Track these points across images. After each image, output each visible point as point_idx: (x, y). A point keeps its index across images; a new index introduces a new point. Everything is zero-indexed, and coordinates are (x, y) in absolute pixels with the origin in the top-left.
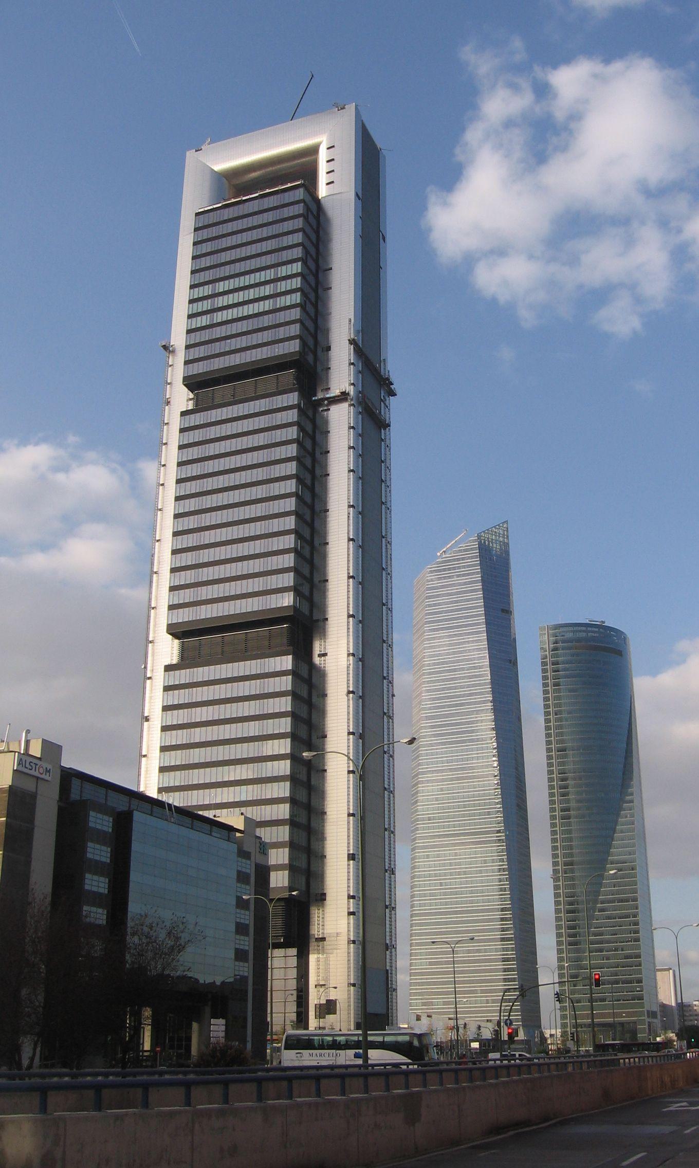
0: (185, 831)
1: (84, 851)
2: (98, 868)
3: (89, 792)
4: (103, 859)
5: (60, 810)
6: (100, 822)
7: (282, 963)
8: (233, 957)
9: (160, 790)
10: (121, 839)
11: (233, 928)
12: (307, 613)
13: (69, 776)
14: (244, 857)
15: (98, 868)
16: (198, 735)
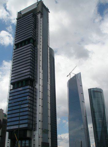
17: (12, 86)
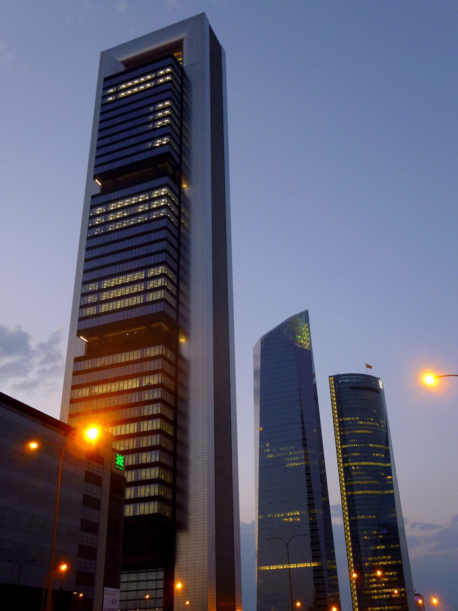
17: (302, 340)
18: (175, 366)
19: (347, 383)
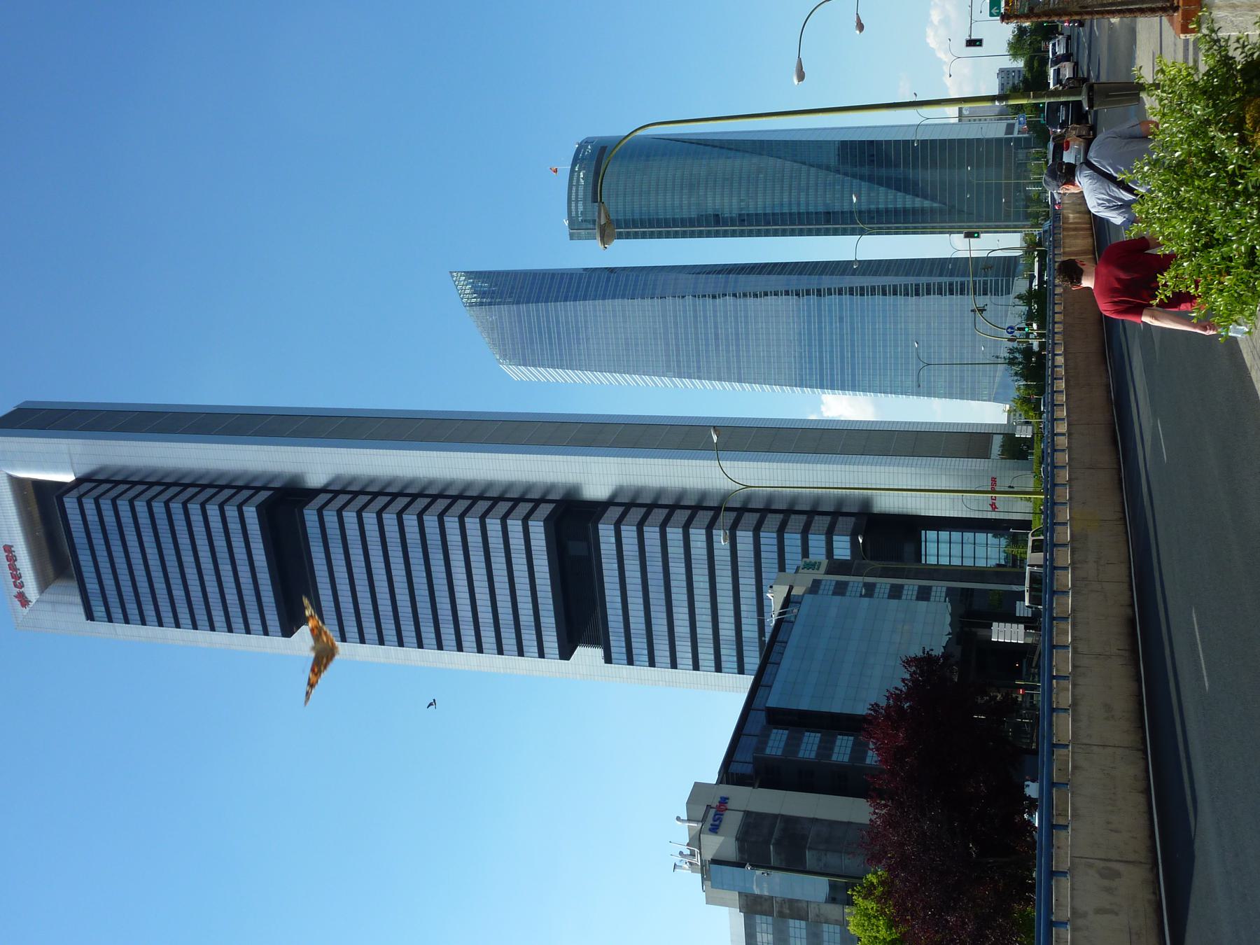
0: (789, 652)
1: (840, 766)
2: (826, 747)
3: (745, 755)
4: (817, 740)
5: (762, 786)
6: (777, 743)
7: (938, 549)
8: (925, 603)
9: (741, 671)
10: (797, 721)
11: (894, 602)
12: (552, 506)
13: (729, 773)
14: (929, 594)
15: (826, 747)
16: (682, 628)
18: (628, 506)
19: (584, 205)
